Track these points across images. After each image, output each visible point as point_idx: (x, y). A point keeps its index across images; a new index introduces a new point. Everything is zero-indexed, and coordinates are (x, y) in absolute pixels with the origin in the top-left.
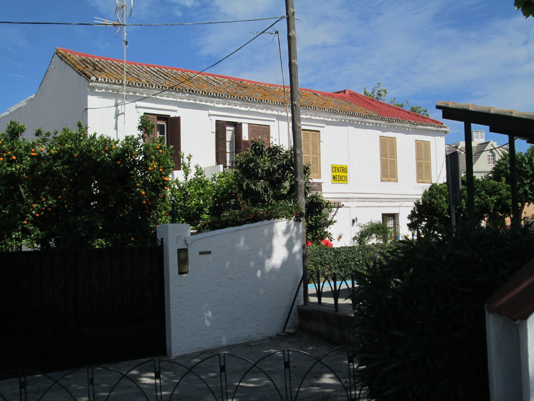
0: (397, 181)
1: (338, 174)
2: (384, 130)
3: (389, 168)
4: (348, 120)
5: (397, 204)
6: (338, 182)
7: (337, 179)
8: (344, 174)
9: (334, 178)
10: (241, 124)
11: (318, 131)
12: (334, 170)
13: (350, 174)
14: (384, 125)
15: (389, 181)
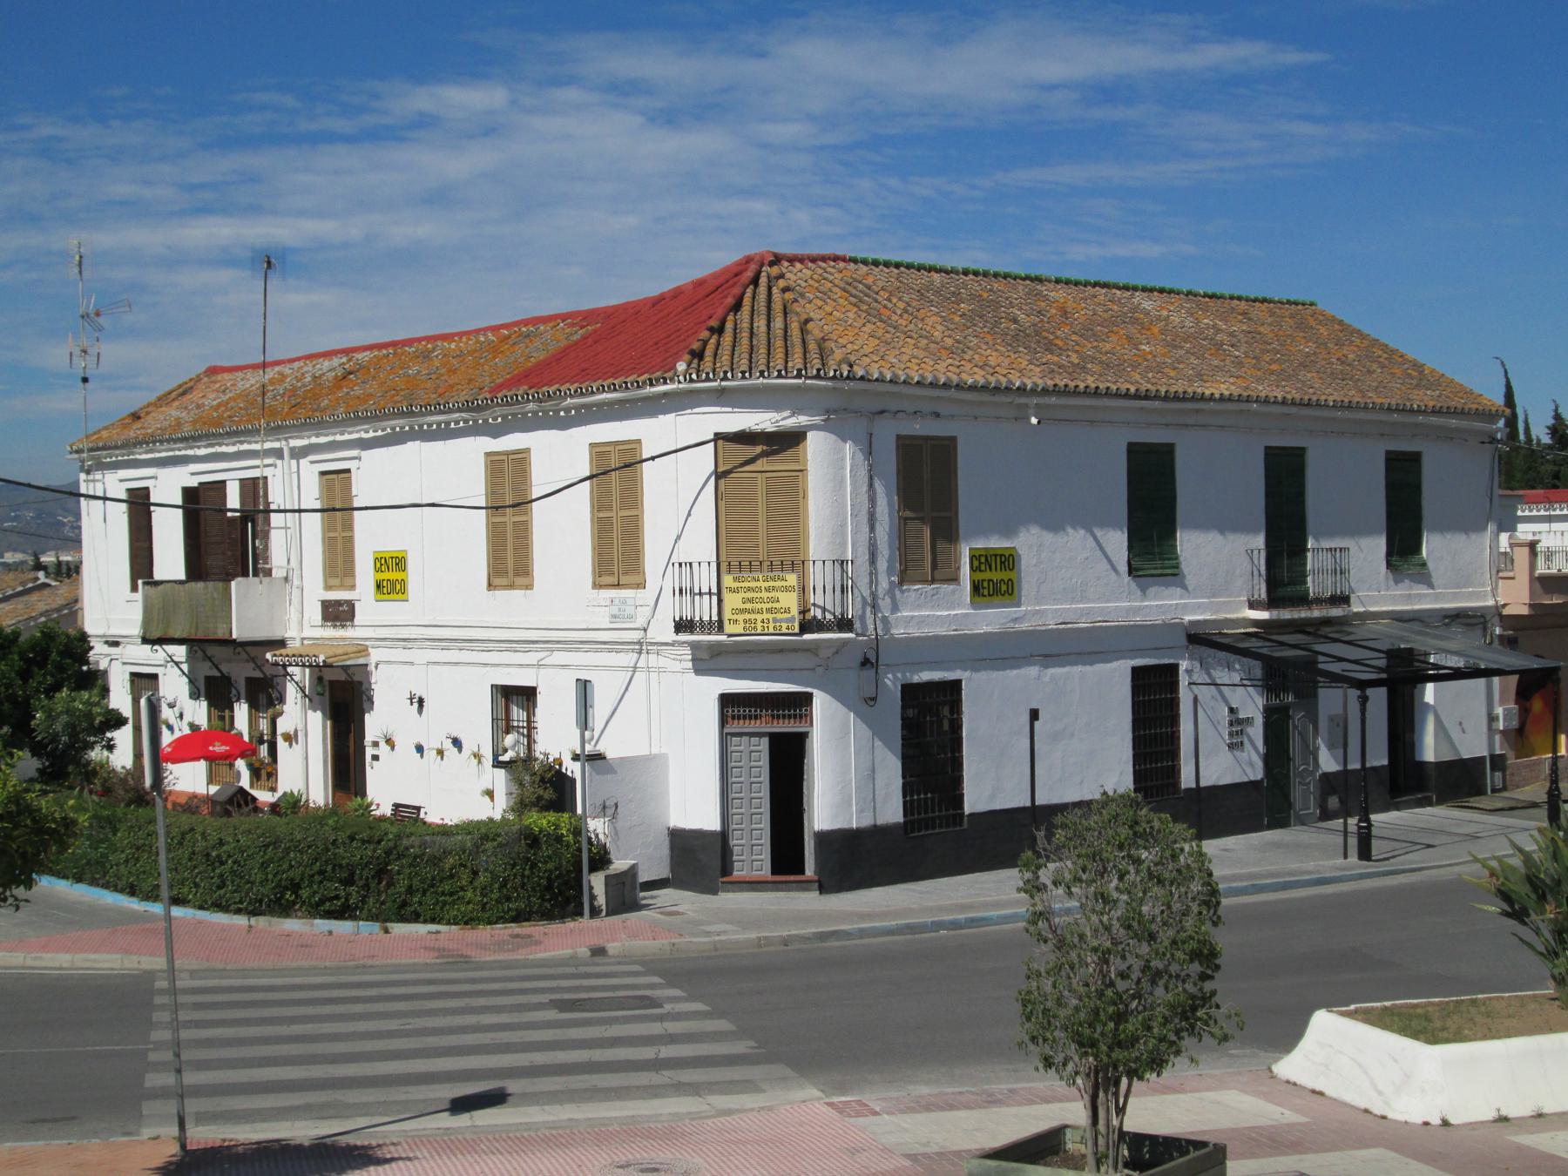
0: (529, 587)
1: (987, 575)
2: (496, 432)
3: (510, 547)
4: (511, 414)
5: (532, 658)
6: (386, 596)
7: (385, 591)
8: (1005, 575)
9: (379, 586)
10: (223, 482)
11: (348, 471)
12: (378, 565)
13: (414, 576)
14: (457, 423)
15: (511, 587)
